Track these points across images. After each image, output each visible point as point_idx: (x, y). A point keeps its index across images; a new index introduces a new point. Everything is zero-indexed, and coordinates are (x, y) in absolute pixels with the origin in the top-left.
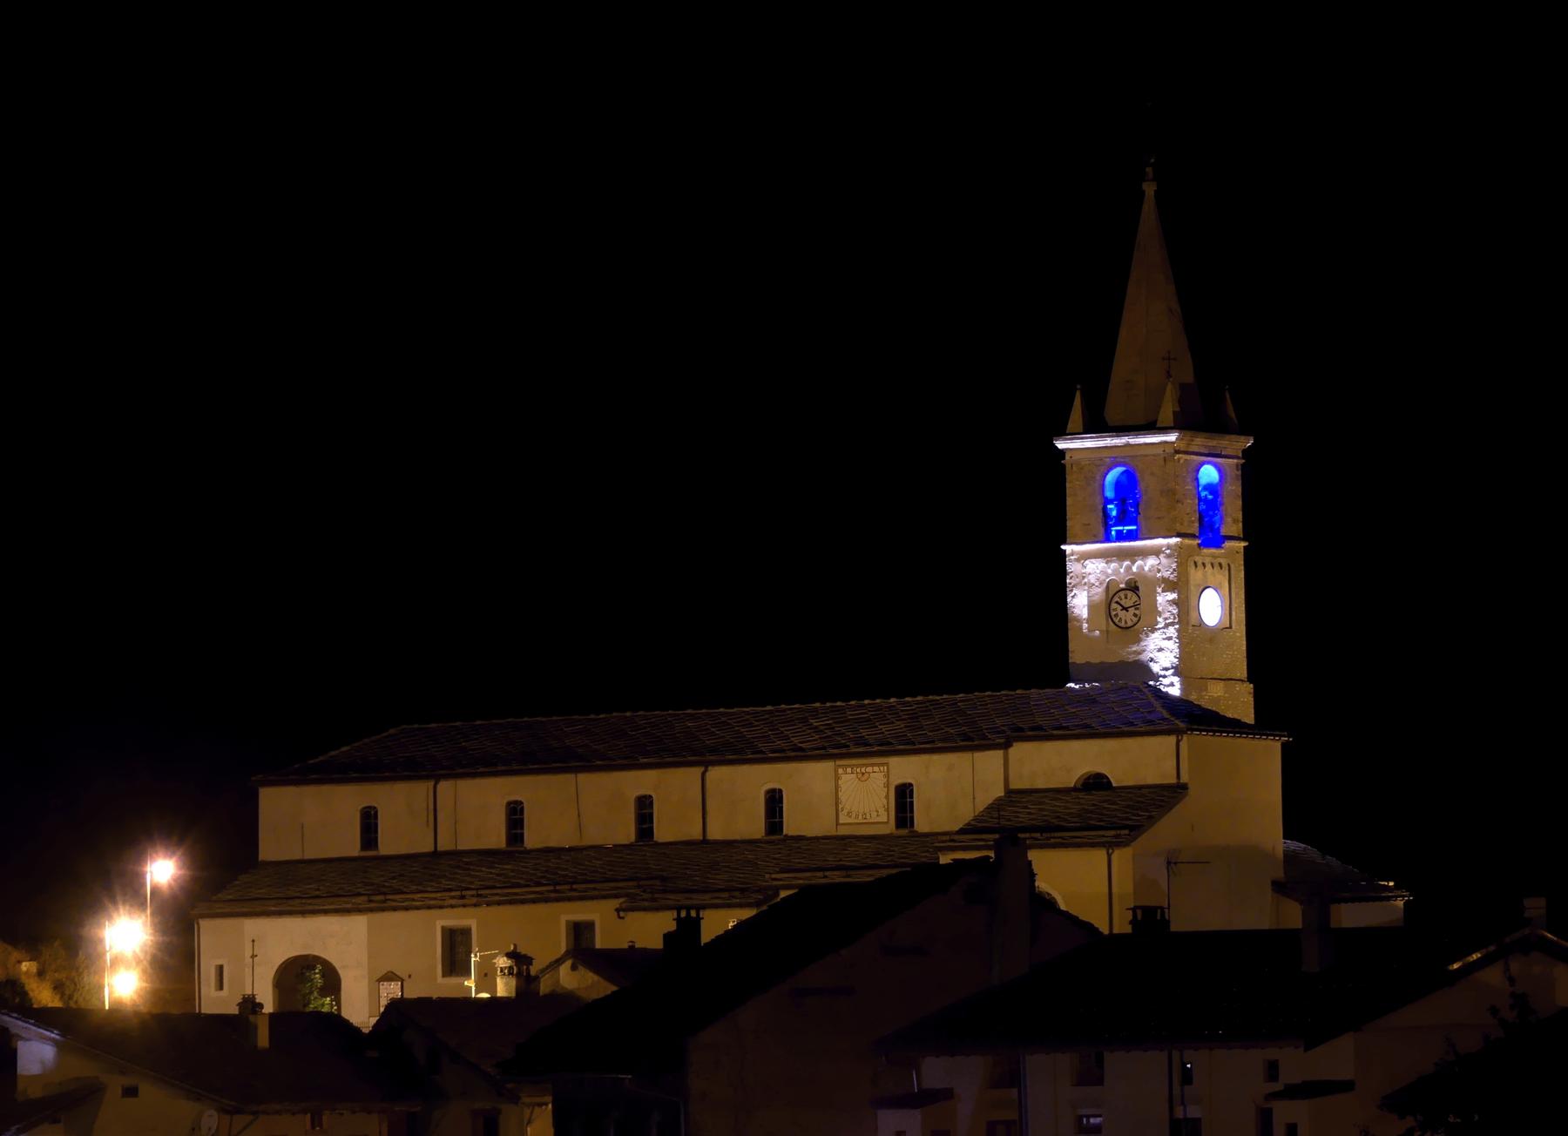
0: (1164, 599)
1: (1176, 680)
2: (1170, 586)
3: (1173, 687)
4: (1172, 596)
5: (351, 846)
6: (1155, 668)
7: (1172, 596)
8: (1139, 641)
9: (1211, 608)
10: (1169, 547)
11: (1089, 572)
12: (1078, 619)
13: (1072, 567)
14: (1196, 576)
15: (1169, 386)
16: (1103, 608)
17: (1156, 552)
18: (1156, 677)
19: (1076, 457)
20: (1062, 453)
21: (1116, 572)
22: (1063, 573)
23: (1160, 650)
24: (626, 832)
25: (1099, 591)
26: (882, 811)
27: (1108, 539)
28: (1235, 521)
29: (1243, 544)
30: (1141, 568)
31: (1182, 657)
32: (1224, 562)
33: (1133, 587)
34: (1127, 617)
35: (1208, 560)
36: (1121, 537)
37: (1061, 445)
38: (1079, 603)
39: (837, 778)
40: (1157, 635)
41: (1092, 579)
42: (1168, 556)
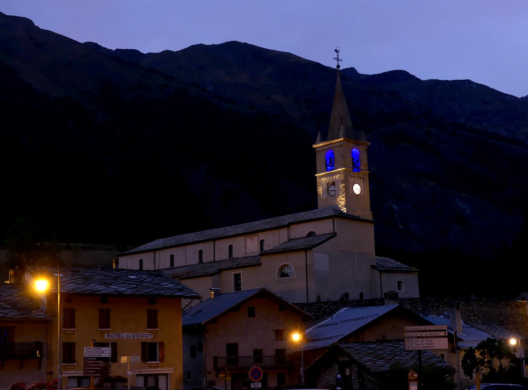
0: (342, 185)
1: (345, 209)
2: (343, 182)
3: (344, 210)
4: (343, 185)
5: (137, 268)
6: (340, 206)
7: (343, 185)
8: (336, 198)
9: (357, 189)
10: (342, 170)
11: (322, 179)
12: (320, 195)
13: (318, 180)
14: (351, 180)
15: (342, 126)
16: (326, 190)
17: (339, 173)
18: (341, 208)
19: (319, 149)
20: (315, 148)
21: (329, 180)
22: (316, 182)
23: (341, 201)
24: (196, 260)
25: (325, 186)
26: (257, 249)
27: (327, 171)
28: (365, 166)
29: (368, 172)
30: (335, 178)
31: (346, 202)
32: (361, 176)
33: (333, 184)
34: (332, 193)
35: (355, 175)
36: (331, 170)
37: (314, 146)
38: (320, 190)
39: (246, 240)
40: (340, 196)
41: (323, 183)
42: (342, 173)
